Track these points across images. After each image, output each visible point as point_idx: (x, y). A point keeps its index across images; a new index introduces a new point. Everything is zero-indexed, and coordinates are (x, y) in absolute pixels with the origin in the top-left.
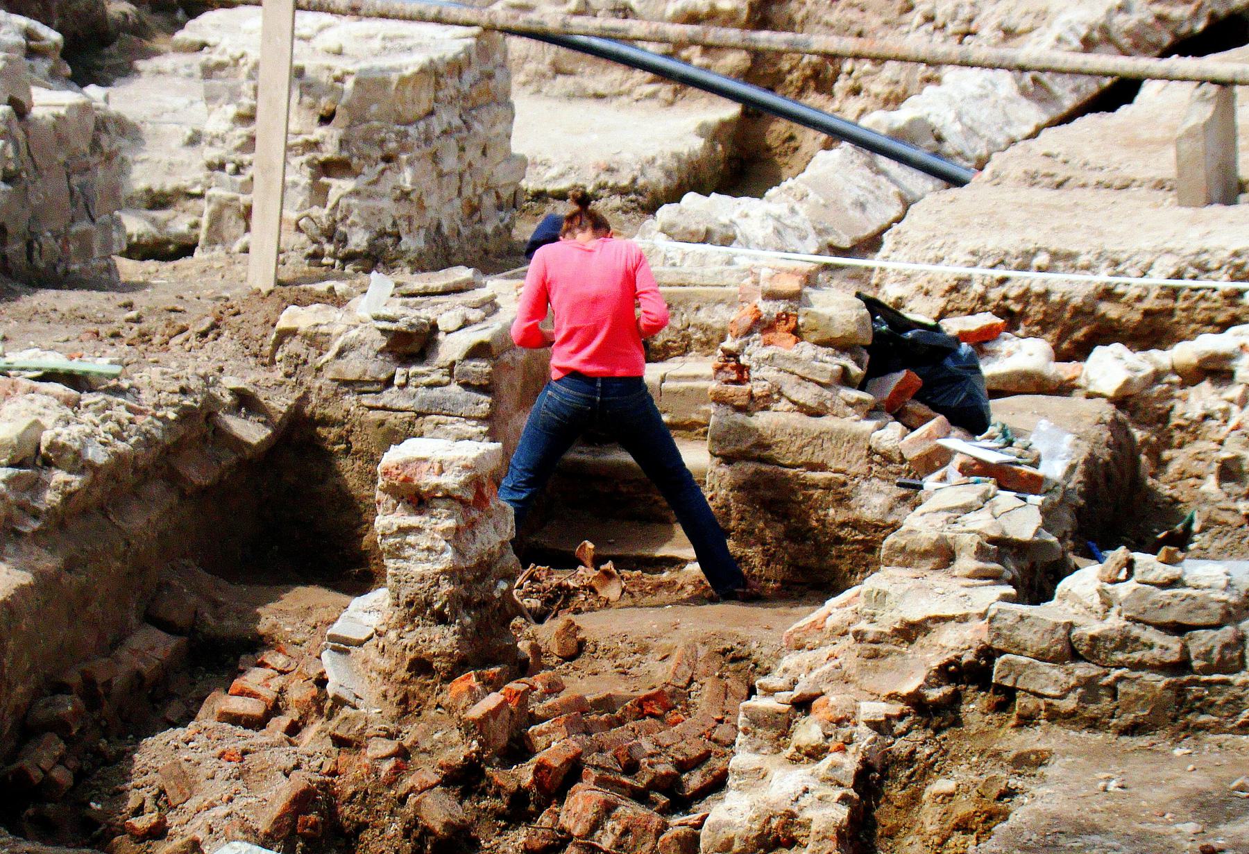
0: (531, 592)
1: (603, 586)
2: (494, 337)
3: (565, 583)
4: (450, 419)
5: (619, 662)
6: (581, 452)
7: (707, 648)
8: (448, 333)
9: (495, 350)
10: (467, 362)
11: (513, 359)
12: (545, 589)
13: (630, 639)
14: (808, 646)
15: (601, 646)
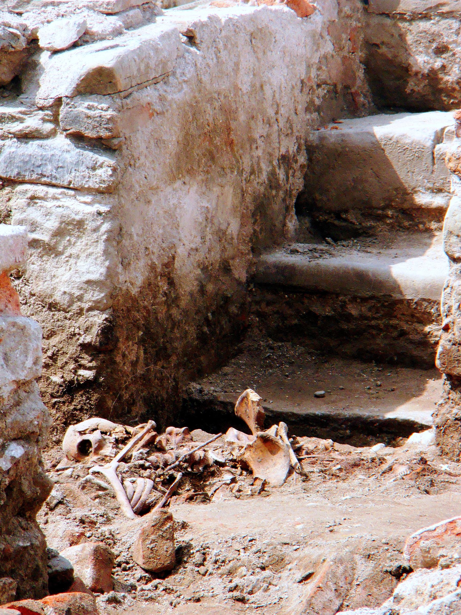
0: (142, 467)
1: (261, 461)
2: (121, 61)
3: (199, 454)
4: (52, 191)
5: (236, 581)
6: (294, 252)
7: (371, 564)
8: (56, 52)
9: (122, 83)
10: (78, 100)
11: (162, 99)
12: (166, 464)
13: (258, 545)
14: (442, 561)
15: (211, 558)
